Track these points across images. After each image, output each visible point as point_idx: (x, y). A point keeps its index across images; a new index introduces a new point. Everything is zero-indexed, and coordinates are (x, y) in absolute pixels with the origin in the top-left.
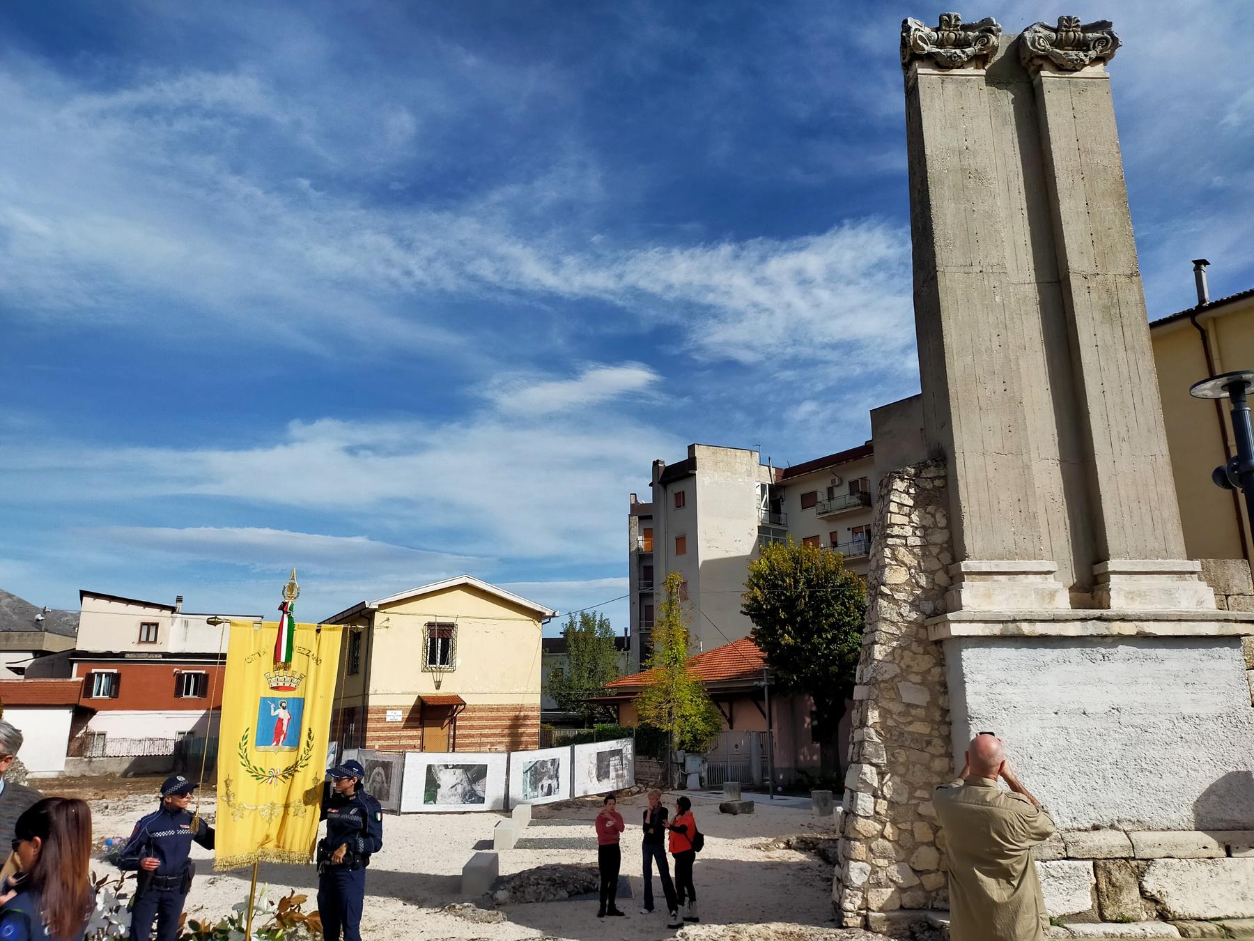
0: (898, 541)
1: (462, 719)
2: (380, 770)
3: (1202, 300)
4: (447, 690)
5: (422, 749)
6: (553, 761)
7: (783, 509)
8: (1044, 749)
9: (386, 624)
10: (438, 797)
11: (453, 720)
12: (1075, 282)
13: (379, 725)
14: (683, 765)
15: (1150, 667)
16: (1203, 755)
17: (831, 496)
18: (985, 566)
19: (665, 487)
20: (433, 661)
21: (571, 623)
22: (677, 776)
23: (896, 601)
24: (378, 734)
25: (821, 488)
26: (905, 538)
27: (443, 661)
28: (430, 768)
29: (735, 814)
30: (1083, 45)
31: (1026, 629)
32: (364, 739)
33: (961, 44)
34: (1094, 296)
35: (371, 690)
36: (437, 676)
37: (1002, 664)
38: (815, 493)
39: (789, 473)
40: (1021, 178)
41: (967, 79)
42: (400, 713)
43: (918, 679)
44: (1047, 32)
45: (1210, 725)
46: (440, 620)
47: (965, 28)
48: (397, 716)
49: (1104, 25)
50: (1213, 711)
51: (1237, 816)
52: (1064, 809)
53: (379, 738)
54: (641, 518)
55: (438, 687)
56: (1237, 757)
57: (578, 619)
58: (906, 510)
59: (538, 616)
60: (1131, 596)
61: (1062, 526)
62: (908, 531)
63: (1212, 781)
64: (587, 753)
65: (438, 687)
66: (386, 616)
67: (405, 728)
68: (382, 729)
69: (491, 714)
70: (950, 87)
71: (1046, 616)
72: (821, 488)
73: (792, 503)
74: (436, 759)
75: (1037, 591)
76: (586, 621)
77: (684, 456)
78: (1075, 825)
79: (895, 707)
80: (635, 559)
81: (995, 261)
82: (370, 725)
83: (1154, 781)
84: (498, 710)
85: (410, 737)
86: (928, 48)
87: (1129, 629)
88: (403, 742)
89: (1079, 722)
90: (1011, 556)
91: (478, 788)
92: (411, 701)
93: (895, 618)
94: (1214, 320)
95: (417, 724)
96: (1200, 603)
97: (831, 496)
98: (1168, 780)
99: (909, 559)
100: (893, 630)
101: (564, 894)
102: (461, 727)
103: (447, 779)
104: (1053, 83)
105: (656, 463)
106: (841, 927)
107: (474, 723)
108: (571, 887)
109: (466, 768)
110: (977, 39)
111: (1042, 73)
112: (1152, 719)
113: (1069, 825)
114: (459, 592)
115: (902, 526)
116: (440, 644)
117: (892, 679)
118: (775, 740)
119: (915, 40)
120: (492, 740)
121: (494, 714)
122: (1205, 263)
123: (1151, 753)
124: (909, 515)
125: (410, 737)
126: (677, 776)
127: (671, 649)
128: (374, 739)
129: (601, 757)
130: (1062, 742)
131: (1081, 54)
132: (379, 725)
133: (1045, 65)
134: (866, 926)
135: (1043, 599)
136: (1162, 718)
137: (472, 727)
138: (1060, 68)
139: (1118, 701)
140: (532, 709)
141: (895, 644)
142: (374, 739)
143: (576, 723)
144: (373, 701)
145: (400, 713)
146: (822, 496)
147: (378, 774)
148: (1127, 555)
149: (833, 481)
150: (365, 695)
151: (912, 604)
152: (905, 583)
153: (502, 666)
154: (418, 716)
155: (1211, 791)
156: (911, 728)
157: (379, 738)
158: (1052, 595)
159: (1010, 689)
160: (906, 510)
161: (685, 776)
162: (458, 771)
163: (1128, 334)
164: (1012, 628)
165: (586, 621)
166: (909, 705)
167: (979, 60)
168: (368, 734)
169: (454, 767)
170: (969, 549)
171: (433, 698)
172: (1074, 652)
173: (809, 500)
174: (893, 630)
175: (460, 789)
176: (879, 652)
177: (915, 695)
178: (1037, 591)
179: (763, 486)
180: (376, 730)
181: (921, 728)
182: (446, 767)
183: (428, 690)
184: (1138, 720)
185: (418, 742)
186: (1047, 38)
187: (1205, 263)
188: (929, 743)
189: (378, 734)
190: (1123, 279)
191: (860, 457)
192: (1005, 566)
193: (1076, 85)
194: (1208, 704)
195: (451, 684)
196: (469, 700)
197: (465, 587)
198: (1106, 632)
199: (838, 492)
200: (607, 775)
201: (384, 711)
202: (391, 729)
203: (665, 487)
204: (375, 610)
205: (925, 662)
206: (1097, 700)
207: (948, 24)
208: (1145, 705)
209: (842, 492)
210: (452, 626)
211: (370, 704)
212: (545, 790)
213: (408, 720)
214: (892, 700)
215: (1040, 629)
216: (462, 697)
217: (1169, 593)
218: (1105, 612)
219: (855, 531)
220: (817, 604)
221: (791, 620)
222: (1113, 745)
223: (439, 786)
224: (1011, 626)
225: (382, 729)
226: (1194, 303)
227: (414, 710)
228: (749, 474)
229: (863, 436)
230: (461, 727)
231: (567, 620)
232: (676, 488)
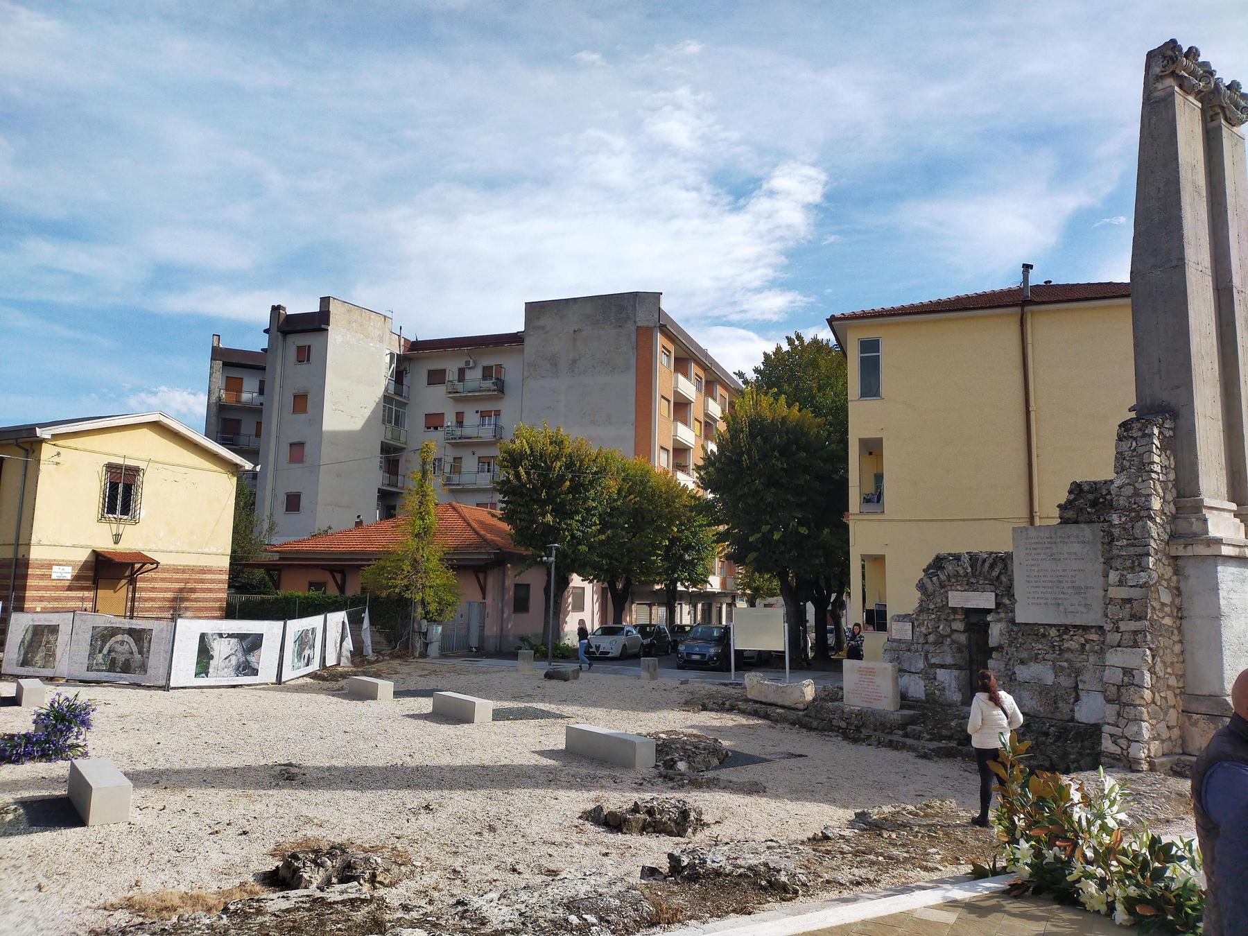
1: (144, 580)
4: (123, 546)
5: (95, 610)
7: (405, 381)
9: (56, 459)
11: (132, 581)
13: (42, 583)
14: (425, 634)
17: (461, 378)
19: (285, 338)
20: (111, 509)
22: (418, 644)
25: (451, 367)
27: (126, 510)
28: (203, 637)
29: (566, 680)
35: (34, 539)
38: (444, 371)
39: (416, 346)
42: (69, 569)
48: (67, 573)
53: (41, 599)
54: (225, 364)
55: (116, 543)
65: (116, 543)
67: (70, 588)
68: (46, 588)
72: (451, 367)
73: (417, 377)
77: (315, 308)
80: (214, 410)
82: (30, 582)
84: (184, 571)
85: (83, 599)
88: (71, 604)
91: (252, 659)
92: (83, 556)
94: (1032, 313)
95: (89, 584)
97: (461, 378)
102: (142, 589)
103: (222, 650)
105: (276, 309)
106: (1133, 771)
107: (157, 585)
109: (241, 637)
114: (145, 432)
116: (121, 492)
118: (489, 610)
122: (1031, 267)
125: (83, 599)
126: (418, 644)
127: (423, 519)
128: (34, 599)
132: (42, 583)
134: (1152, 768)
137: (153, 589)
140: (221, 572)
142: (34, 599)
144: (36, 554)
145: (69, 569)
146: (452, 375)
149: (467, 363)
154: (91, 574)
157: (41, 599)
161: (426, 645)
162: (233, 641)
168: (28, 594)
169: (230, 636)
173: (436, 377)
175: (234, 660)
179: (392, 355)
180: (39, 589)
182: (221, 635)
183: (105, 544)
185: (89, 605)
191: (502, 344)
195: (133, 538)
197: (157, 426)
199: (469, 375)
201: (49, 566)
202: (57, 588)
203: (285, 338)
209: (474, 376)
210: (134, 472)
211: (32, 556)
213: (76, 578)
219: (484, 414)
220: (576, 488)
221: (550, 500)
223: (212, 657)
225: (46, 588)
227: (85, 566)
228: (381, 340)
229: (516, 324)
230: (142, 589)
232: (303, 340)
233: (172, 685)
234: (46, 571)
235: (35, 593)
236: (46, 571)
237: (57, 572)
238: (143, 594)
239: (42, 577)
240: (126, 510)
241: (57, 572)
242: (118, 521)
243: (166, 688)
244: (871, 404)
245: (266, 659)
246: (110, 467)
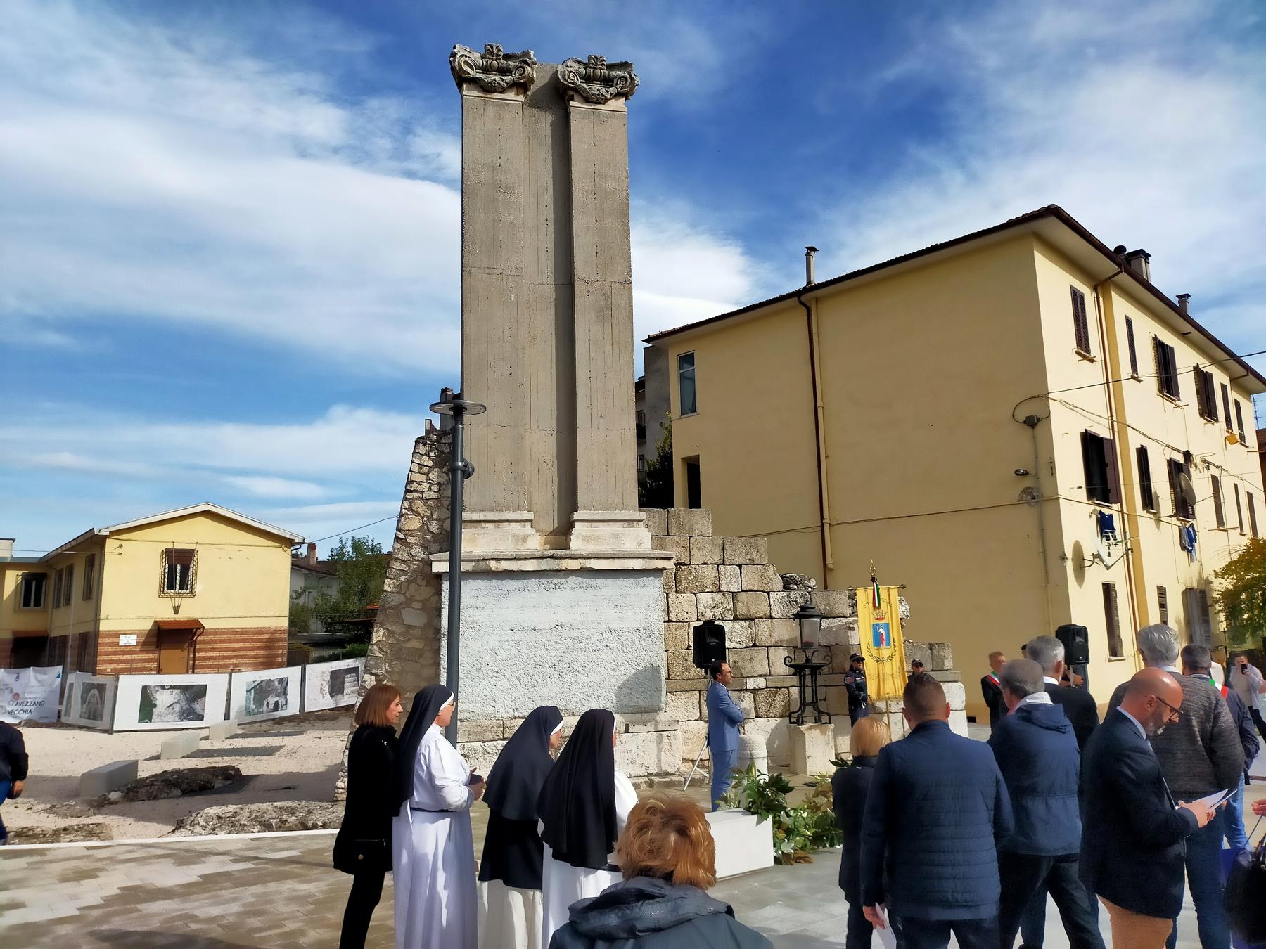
0: (416, 495)
1: (201, 642)
2: (95, 692)
3: (809, 282)
4: (184, 615)
6: (281, 680)
8: (500, 657)
9: (119, 550)
10: (154, 716)
11: (193, 643)
12: (578, 286)
13: (110, 649)
15: (590, 592)
16: (621, 659)
18: (475, 516)
20: (171, 586)
21: (342, 548)
23: (407, 544)
24: (110, 658)
26: (422, 492)
27: (37, 603)
28: (145, 688)
30: (608, 81)
31: (493, 565)
32: (95, 663)
33: (503, 71)
34: (592, 298)
35: (102, 615)
36: (177, 601)
37: (474, 593)
40: (551, 192)
41: (506, 104)
42: (135, 637)
43: (418, 606)
44: (576, 66)
45: (630, 636)
46: (177, 547)
47: (508, 57)
48: (132, 640)
49: (625, 65)
50: (634, 625)
51: (641, 702)
52: (509, 702)
53: (111, 662)
56: (647, 658)
57: (350, 543)
58: (425, 469)
59: (287, 542)
60: (587, 539)
61: (550, 483)
62: (426, 486)
63: (625, 678)
64: (319, 673)
66: (120, 542)
67: (142, 652)
69: (233, 637)
70: (491, 110)
71: (510, 555)
74: (152, 680)
75: (513, 536)
76: (357, 546)
78: (516, 714)
79: (396, 629)
81: (514, 265)
82: (101, 649)
83: (582, 679)
86: (472, 73)
87: (574, 565)
89: (532, 637)
90: (499, 508)
91: (197, 706)
92: (148, 625)
93: (406, 557)
96: (640, 544)
98: (592, 677)
99: (422, 510)
100: (403, 567)
101: (179, 792)
102: (201, 650)
103: (163, 700)
104: (580, 113)
107: (216, 646)
108: (185, 786)
109: (184, 688)
110: (517, 68)
111: (571, 103)
112: (586, 632)
113: (512, 714)
115: (420, 483)
116: (179, 569)
117: (398, 606)
119: (460, 65)
120: (234, 661)
121: (237, 637)
122: (815, 250)
123: (582, 658)
124: (427, 474)
129: (334, 674)
130: (515, 652)
131: (603, 90)
132: (110, 649)
133: (576, 97)
135: (517, 541)
136: (594, 631)
137: (214, 650)
138: (587, 100)
139: (561, 620)
141: (403, 578)
143: (340, 643)
144: (104, 626)
145: (135, 637)
147: (93, 696)
148: (592, 507)
150: (97, 620)
151: (422, 546)
152: (418, 529)
153: (247, 591)
155: (624, 685)
156: (408, 645)
157: (111, 662)
158: (525, 539)
159: (478, 612)
160: (425, 469)
162: (176, 692)
163: (616, 331)
164: (482, 565)
165: (357, 546)
166: (409, 627)
167: (522, 86)
168: (99, 658)
169: (172, 687)
170: (466, 503)
171: (170, 622)
172: (533, 582)
174: (403, 567)
175: (177, 708)
176: (388, 586)
177: (413, 617)
178: (513, 536)
181: (415, 644)
182: (163, 687)
184: (575, 634)
185: (155, 665)
186: (577, 73)
187: (815, 250)
188: (421, 656)
189: (110, 658)
190: (617, 286)
192: (491, 515)
193: (599, 115)
194: (631, 620)
195: (190, 610)
196: (208, 624)
198: (556, 568)
200: (341, 691)
202: (124, 653)
204: (106, 537)
205: (426, 592)
206: (545, 619)
207: (491, 53)
208: (582, 622)
212: (271, 707)
213: (144, 644)
214: (395, 623)
215: (505, 565)
216: (203, 622)
217: (616, 537)
218: (567, 552)
222: (553, 653)
223: (155, 706)
224: (482, 563)
226: (802, 284)
230: (201, 650)
231: (337, 545)
233: (115, 729)
234: (115, 640)
235: (105, 658)
236: (115, 640)
237: (123, 640)
238: (202, 654)
239: (111, 644)
240: (37, 603)
241: (123, 640)
242: (179, 595)
243: (110, 731)
244: (691, 420)
245: (213, 707)
246: (168, 552)
